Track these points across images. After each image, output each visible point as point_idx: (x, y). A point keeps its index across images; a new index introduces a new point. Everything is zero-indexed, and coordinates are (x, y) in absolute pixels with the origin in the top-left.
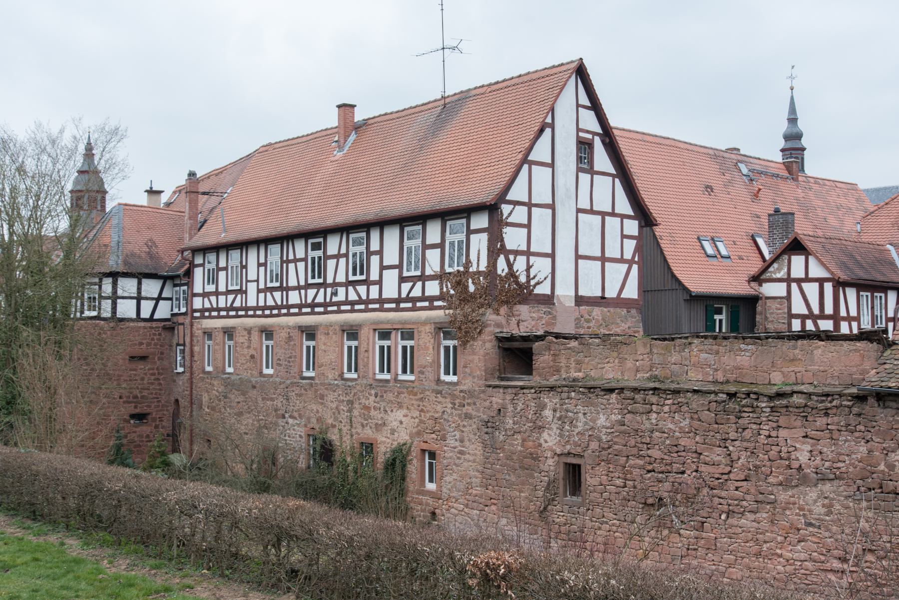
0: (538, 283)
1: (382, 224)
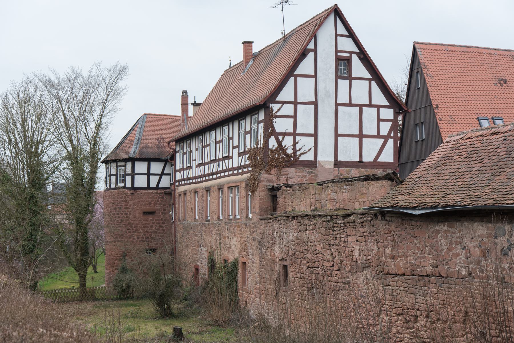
0: (303, 153)
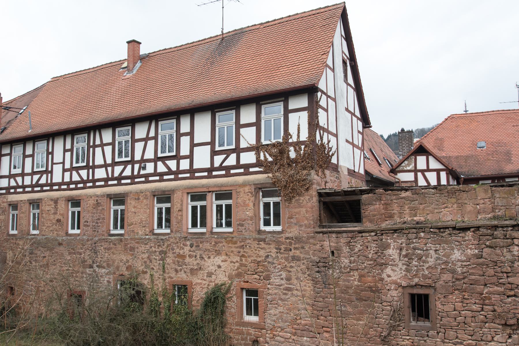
1: (192, 111)
